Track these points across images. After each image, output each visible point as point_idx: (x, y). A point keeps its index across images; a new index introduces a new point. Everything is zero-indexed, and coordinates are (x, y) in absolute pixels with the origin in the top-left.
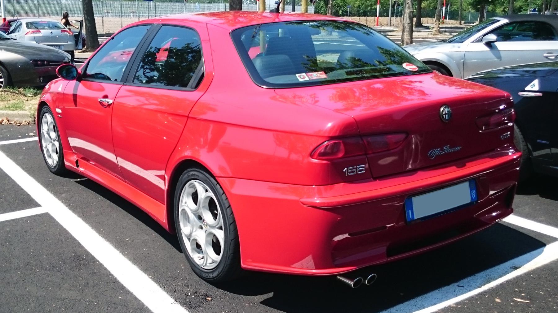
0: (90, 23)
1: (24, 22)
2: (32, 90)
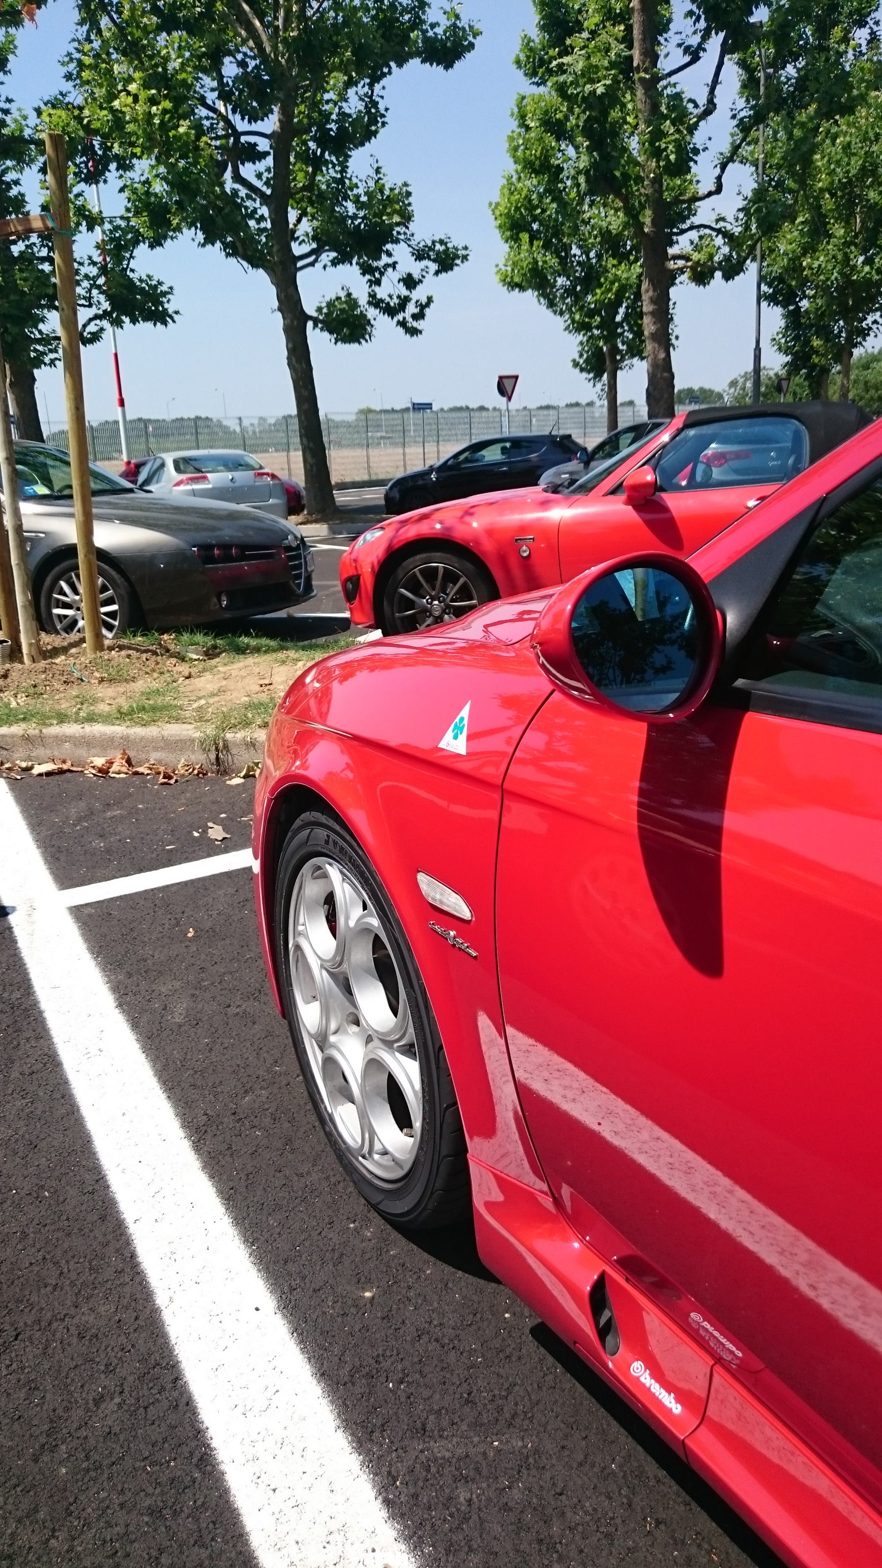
0: (313, 456)
1: (169, 459)
2: (199, 638)
